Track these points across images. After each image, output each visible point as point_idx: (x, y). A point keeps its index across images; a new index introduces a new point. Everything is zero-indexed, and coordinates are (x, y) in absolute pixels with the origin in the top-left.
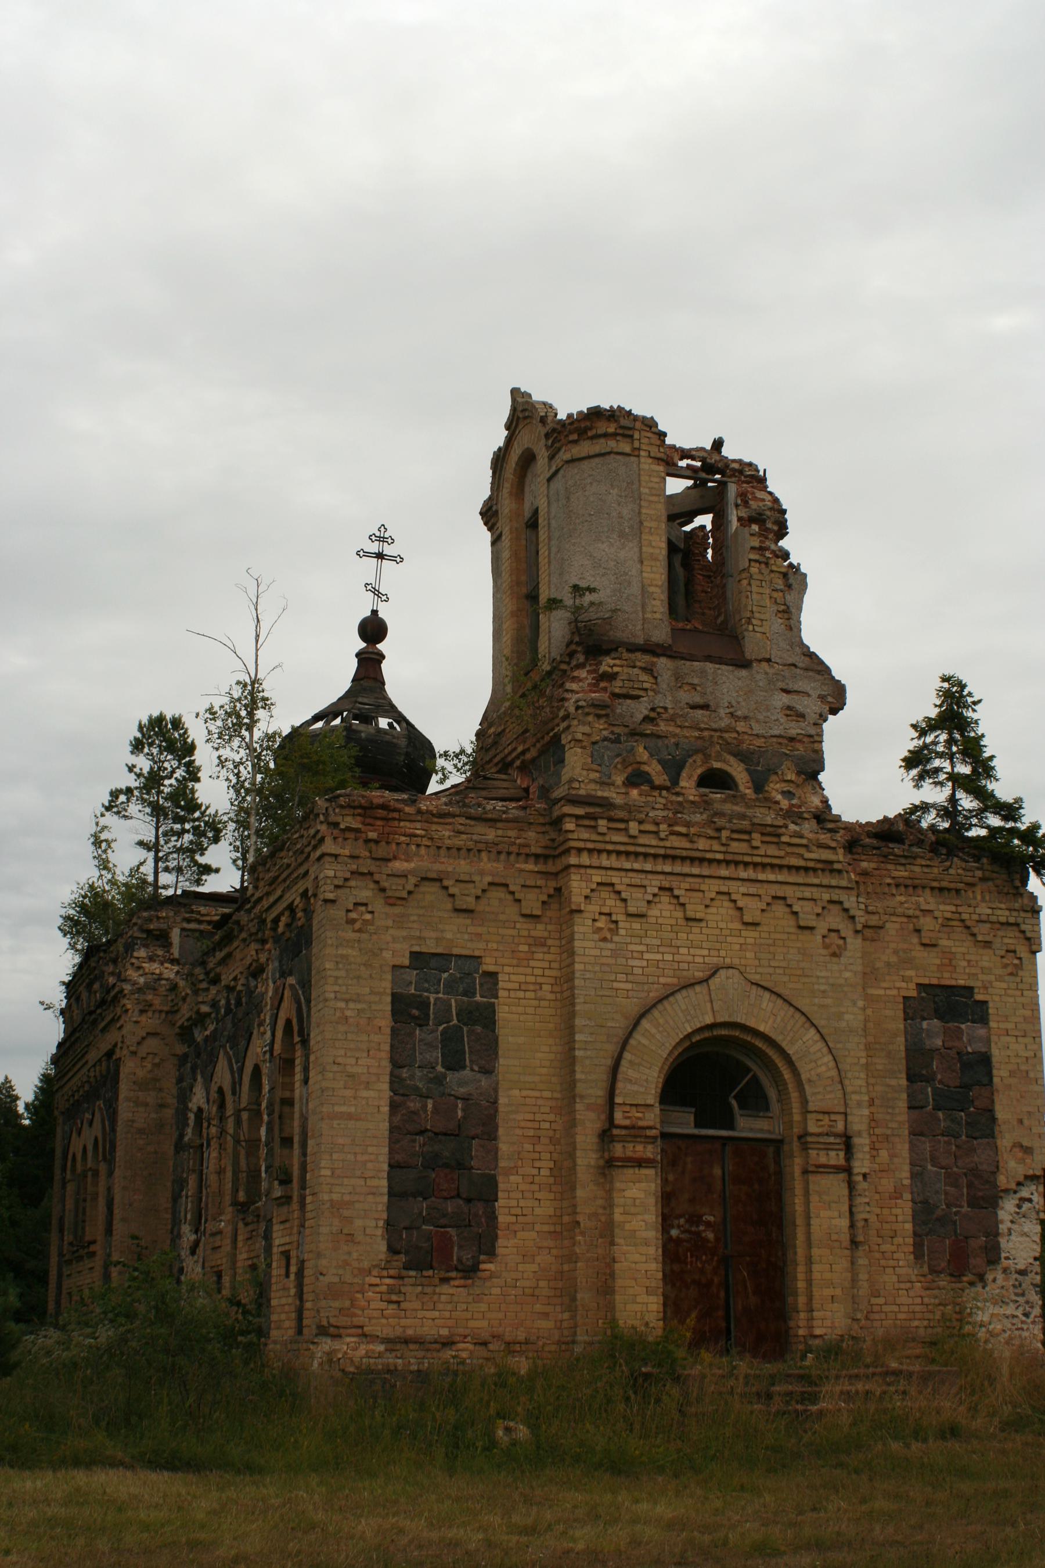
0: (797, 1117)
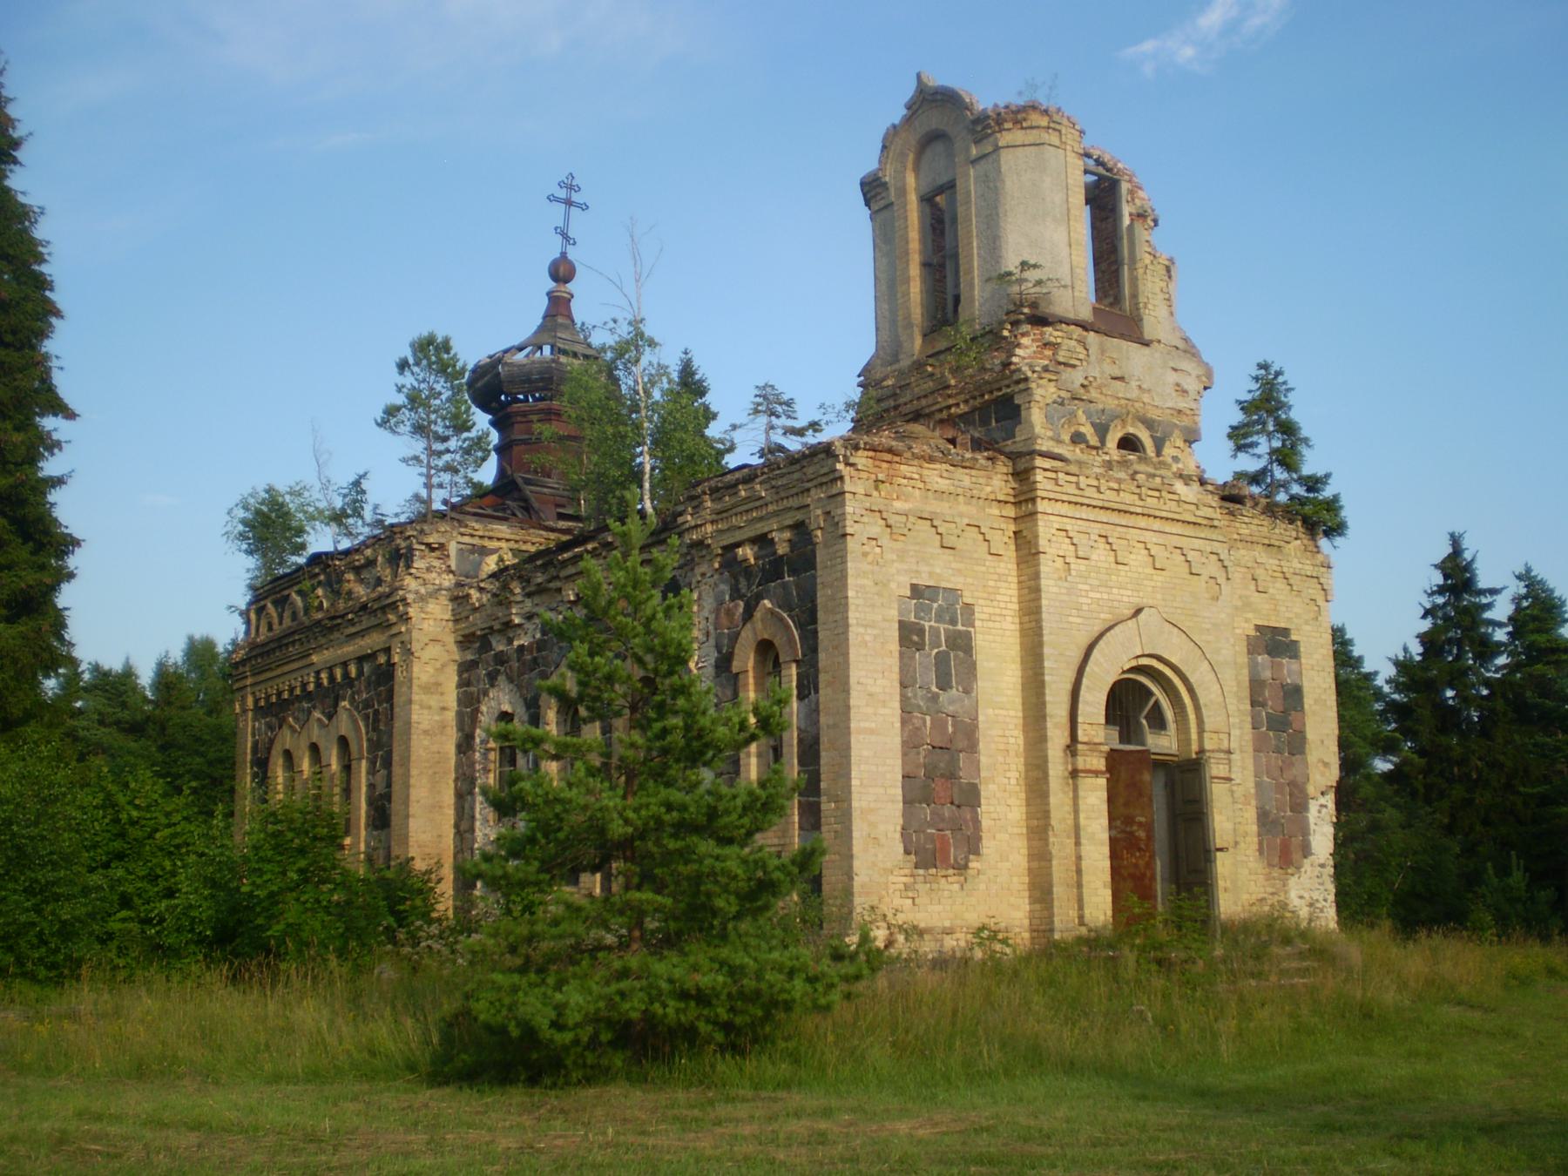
0: (1194, 736)
